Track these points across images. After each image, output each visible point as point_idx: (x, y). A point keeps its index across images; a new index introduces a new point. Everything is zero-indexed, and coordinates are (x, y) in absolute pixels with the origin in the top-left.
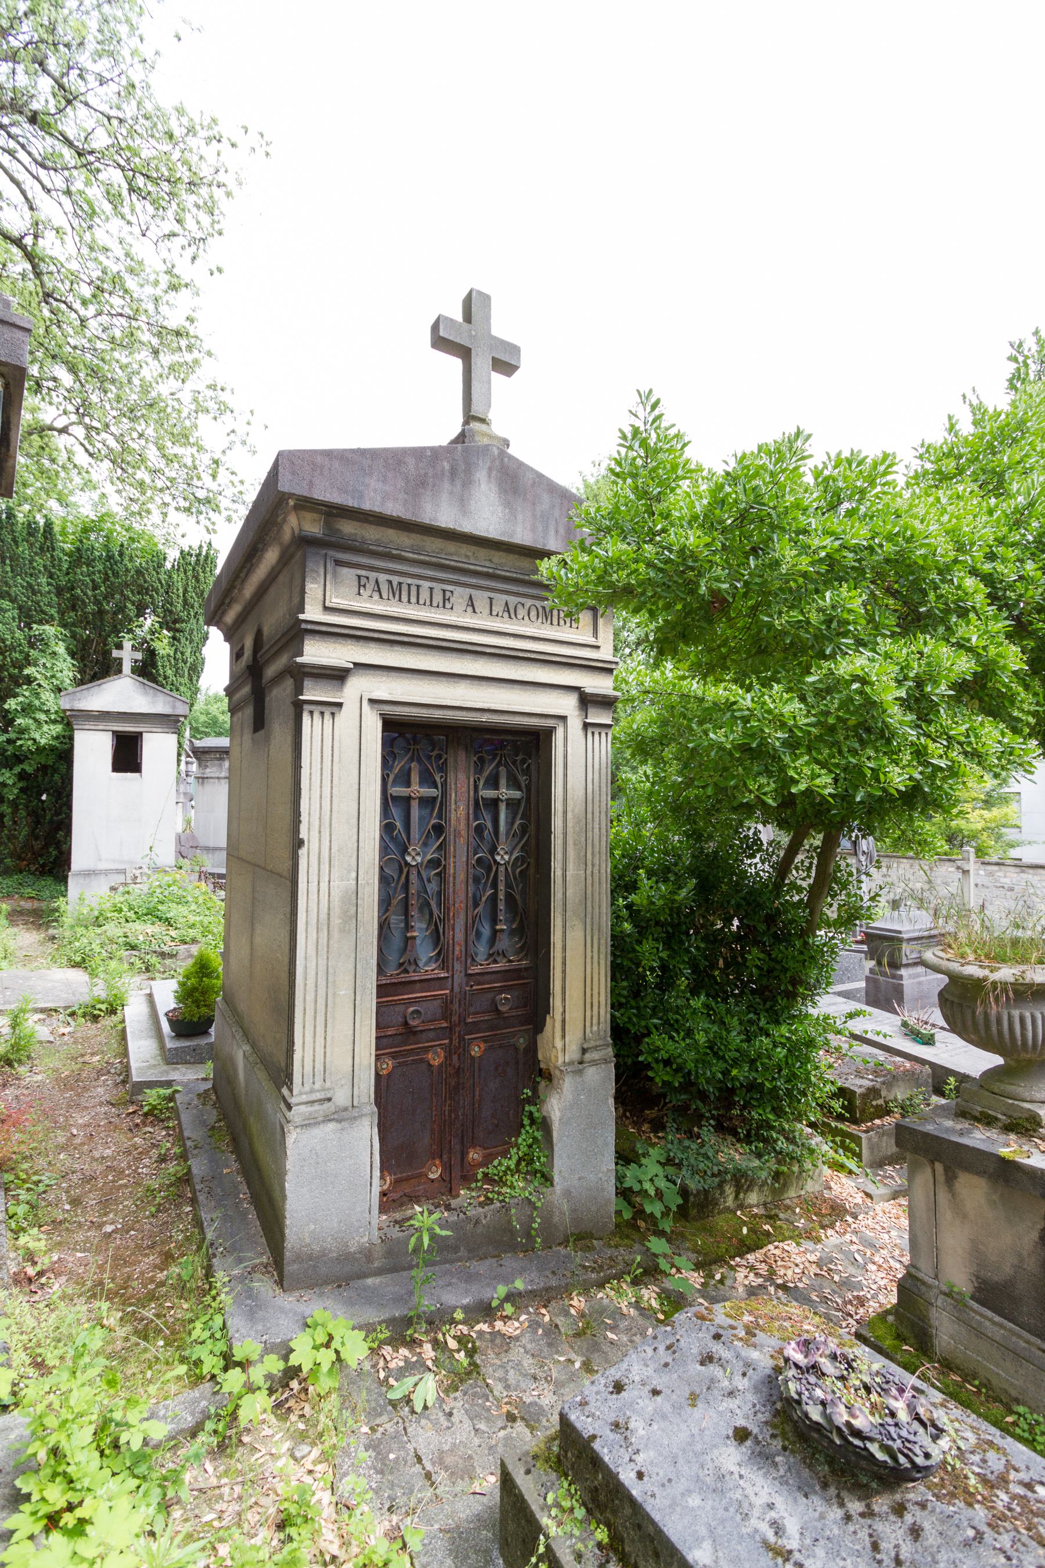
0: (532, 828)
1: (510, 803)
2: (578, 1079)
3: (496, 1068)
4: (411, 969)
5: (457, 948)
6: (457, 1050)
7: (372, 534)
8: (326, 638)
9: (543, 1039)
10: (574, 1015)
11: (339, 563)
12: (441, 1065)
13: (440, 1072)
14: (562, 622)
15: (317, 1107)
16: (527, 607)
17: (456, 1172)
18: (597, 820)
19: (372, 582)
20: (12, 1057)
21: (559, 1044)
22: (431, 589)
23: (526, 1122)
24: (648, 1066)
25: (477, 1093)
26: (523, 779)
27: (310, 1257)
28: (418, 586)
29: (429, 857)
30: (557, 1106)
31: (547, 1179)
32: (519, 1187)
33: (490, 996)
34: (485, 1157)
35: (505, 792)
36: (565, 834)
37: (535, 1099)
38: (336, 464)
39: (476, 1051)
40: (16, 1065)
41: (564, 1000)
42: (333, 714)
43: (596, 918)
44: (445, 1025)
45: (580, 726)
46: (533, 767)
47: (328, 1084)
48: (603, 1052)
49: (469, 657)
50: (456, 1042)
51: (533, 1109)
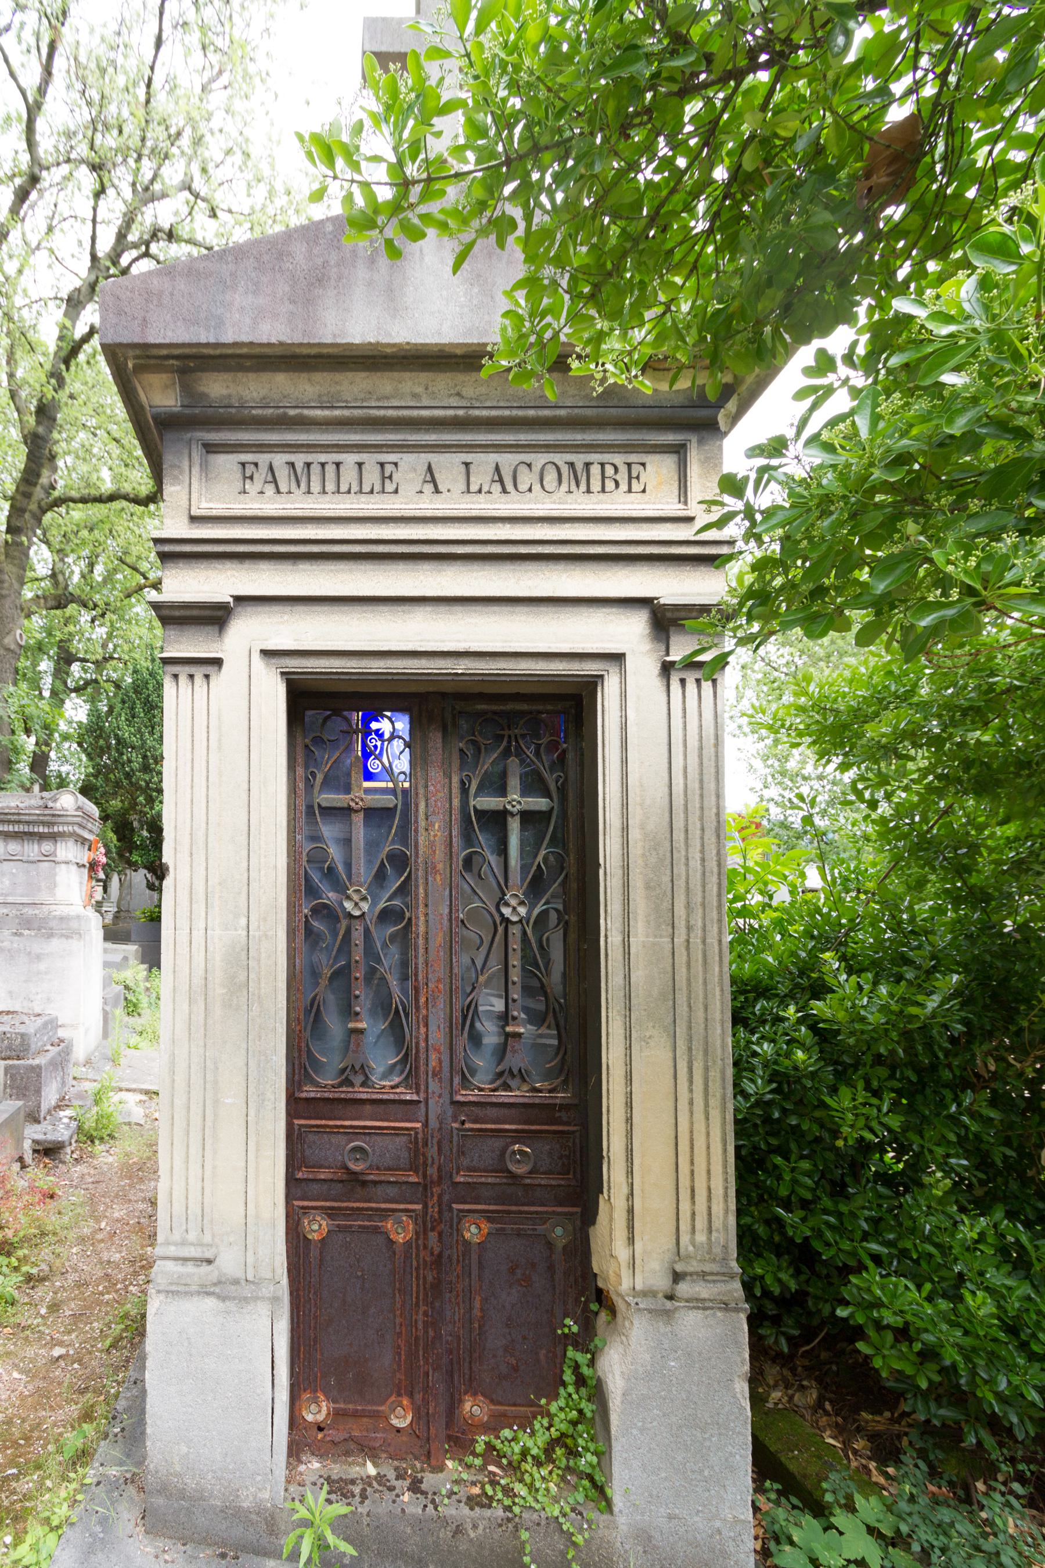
0: (572, 859)
1: (528, 817)
2: (663, 1328)
3: (512, 1271)
4: (358, 1079)
5: (433, 1057)
6: (436, 1223)
7: (253, 390)
8: (194, 563)
9: (599, 1233)
10: (654, 1202)
11: (210, 448)
12: (408, 1244)
13: (407, 1256)
14: (610, 485)
15: (190, 1268)
16: (537, 468)
17: (438, 1429)
18: (696, 843)
19: (264, 469)
20: (95, 1134)
21: (622, 1252)
22: (360, 465)
23: (568, 1376)
24: (859, 1333)
25: (477, 1304)
26: (550, 779)
27: (182, 1495)
28: (338, 465)
29: (382, 905)
30: (622, 1362)
31: (600, 1492)
32: (544, 1495)
33: (498, 1143)
34: (493, 1416)
35: (516, 800)
36: (626, 868)
37: (586, 1340)
38: (181, 285)
39: (472, 1232)
40: (97, 1142)
41: (630, 1173)
42: (207, 676)
43: (699, 1028)
44: (414, 1179)
45: (655, 668)
46: (570, 755)
47: (207, 1238)
48: (721, 1287)
49: (426, 566)
50: (433, 1211)
51: (582, 1358)
